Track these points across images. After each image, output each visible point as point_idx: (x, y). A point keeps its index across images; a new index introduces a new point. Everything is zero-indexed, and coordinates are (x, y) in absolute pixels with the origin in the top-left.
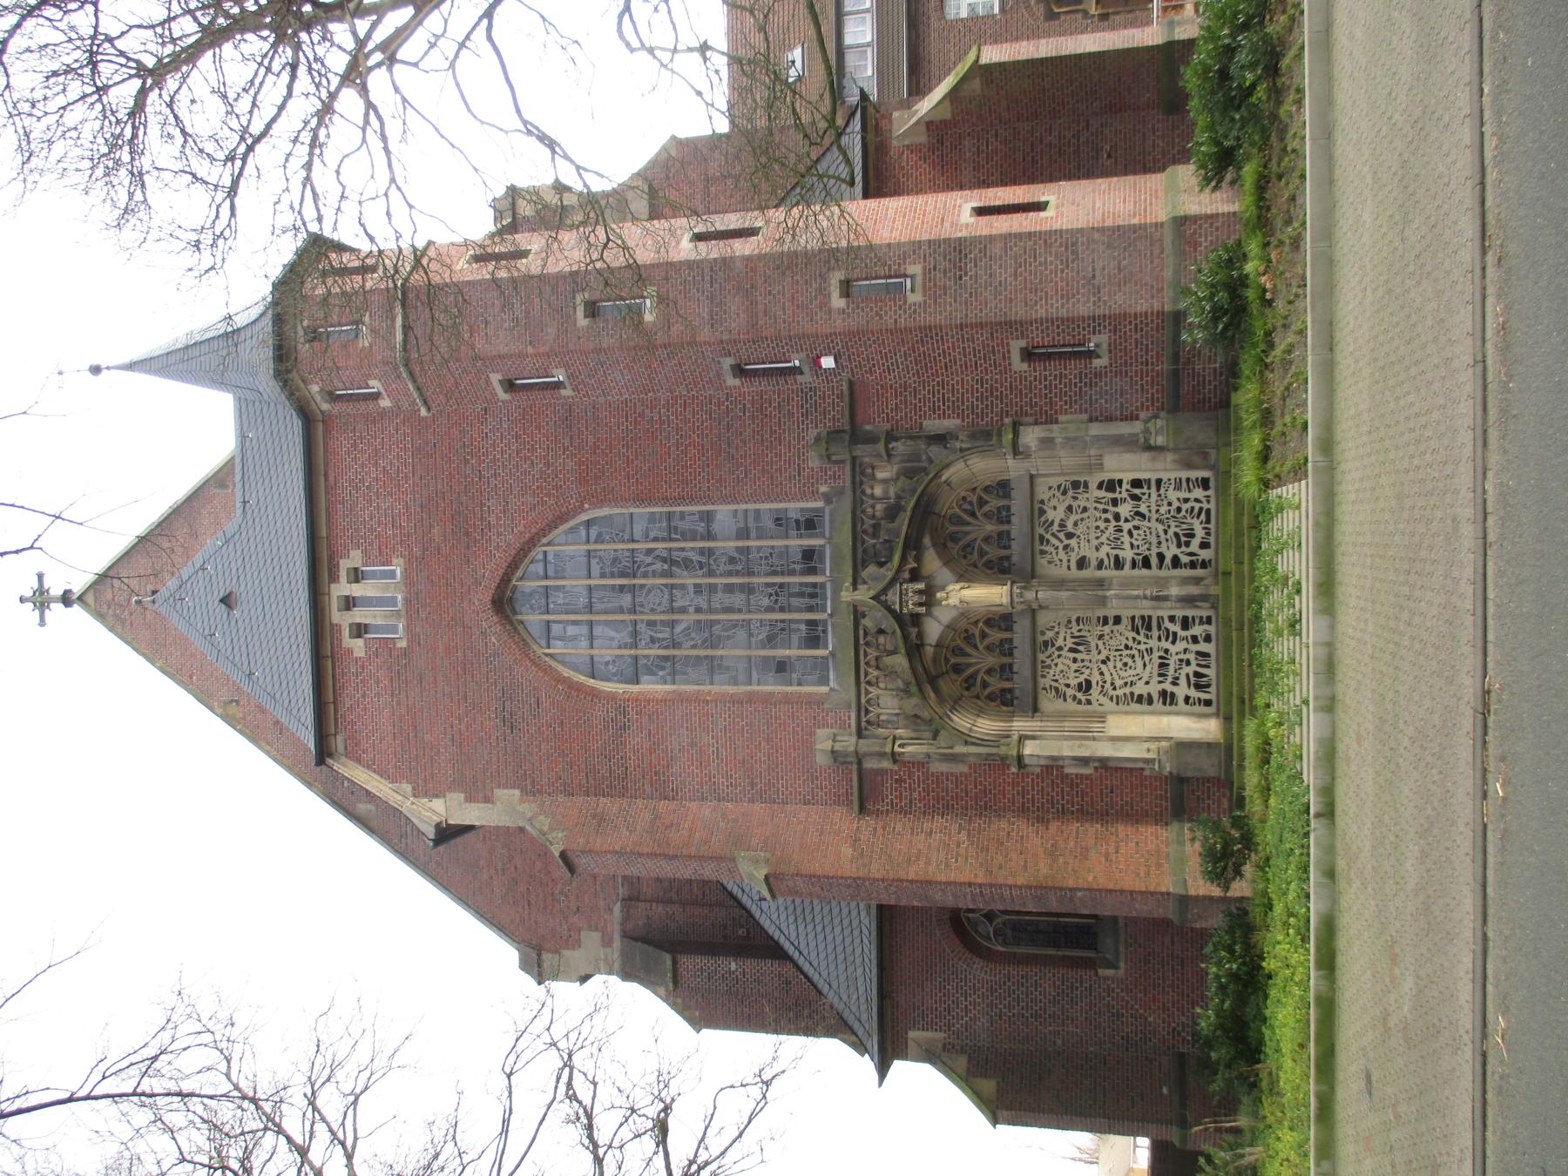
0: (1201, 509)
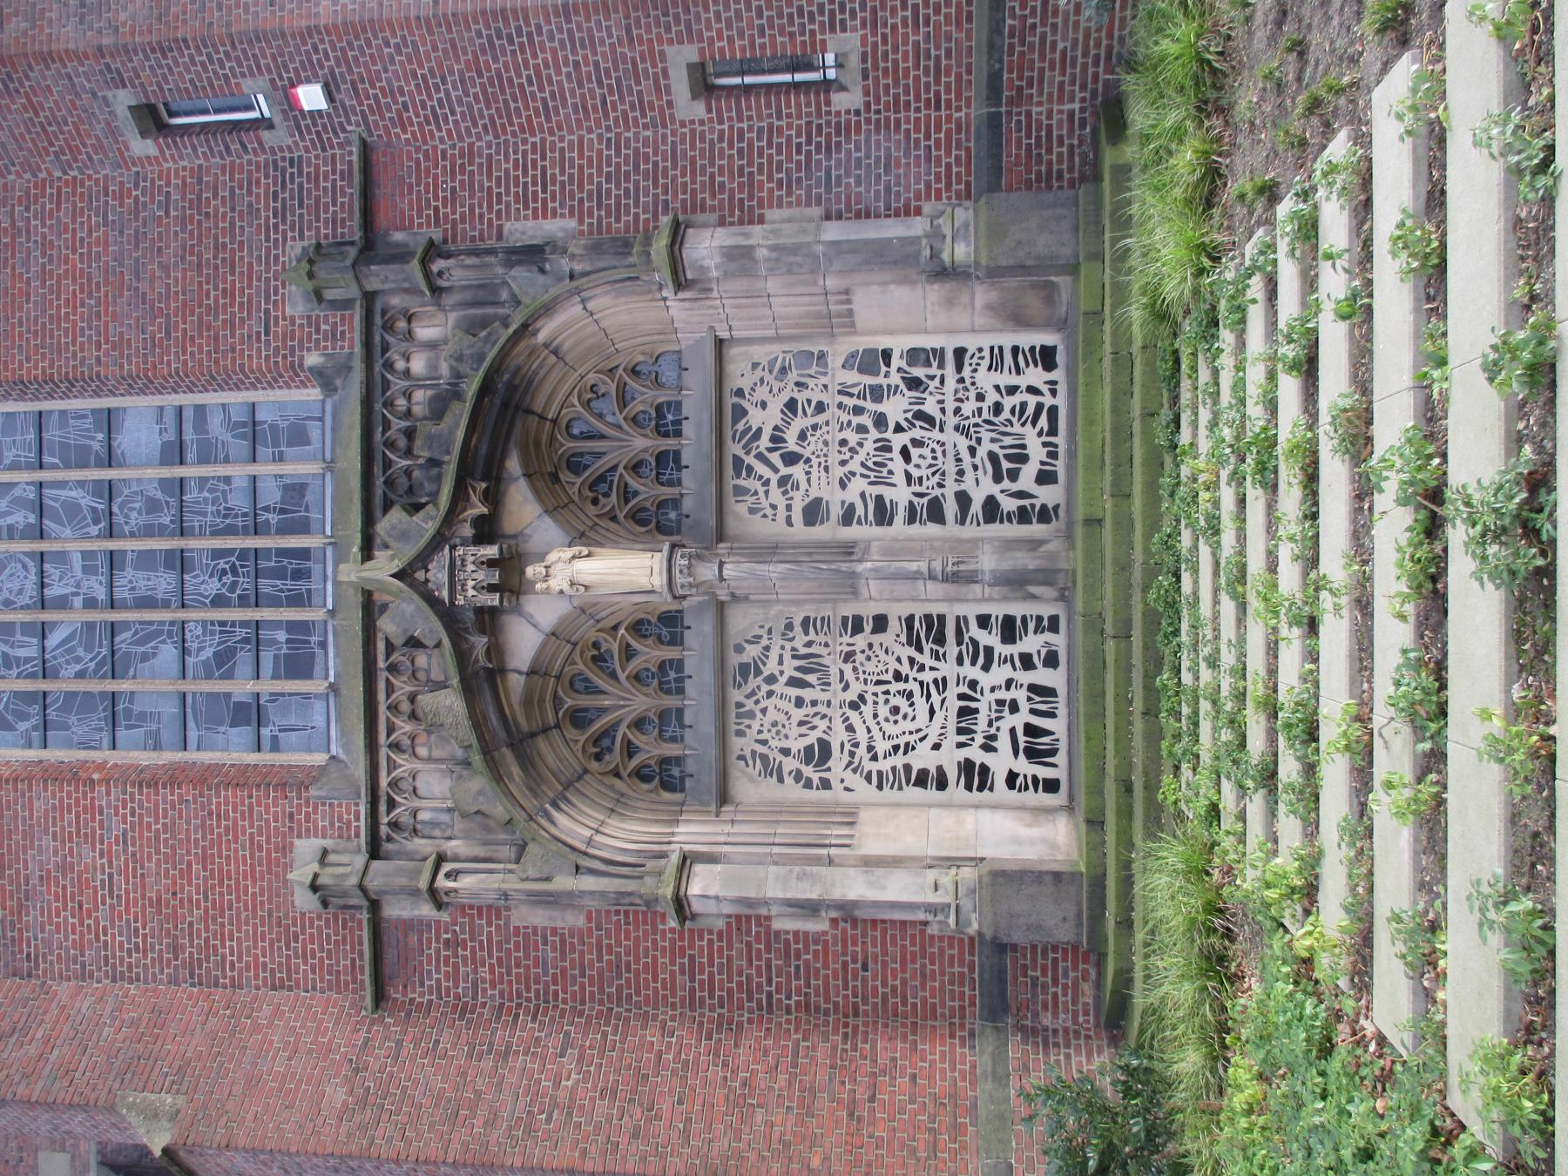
0: (1039, 407)
